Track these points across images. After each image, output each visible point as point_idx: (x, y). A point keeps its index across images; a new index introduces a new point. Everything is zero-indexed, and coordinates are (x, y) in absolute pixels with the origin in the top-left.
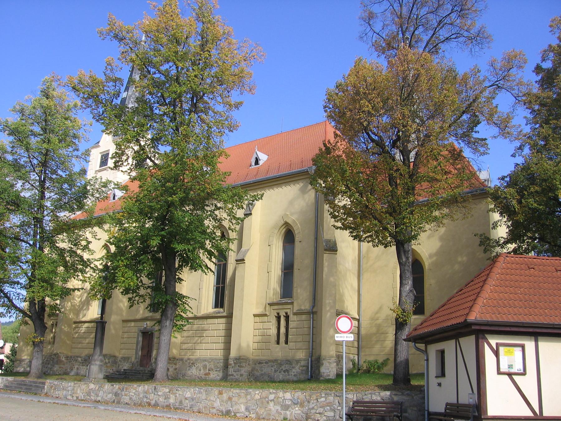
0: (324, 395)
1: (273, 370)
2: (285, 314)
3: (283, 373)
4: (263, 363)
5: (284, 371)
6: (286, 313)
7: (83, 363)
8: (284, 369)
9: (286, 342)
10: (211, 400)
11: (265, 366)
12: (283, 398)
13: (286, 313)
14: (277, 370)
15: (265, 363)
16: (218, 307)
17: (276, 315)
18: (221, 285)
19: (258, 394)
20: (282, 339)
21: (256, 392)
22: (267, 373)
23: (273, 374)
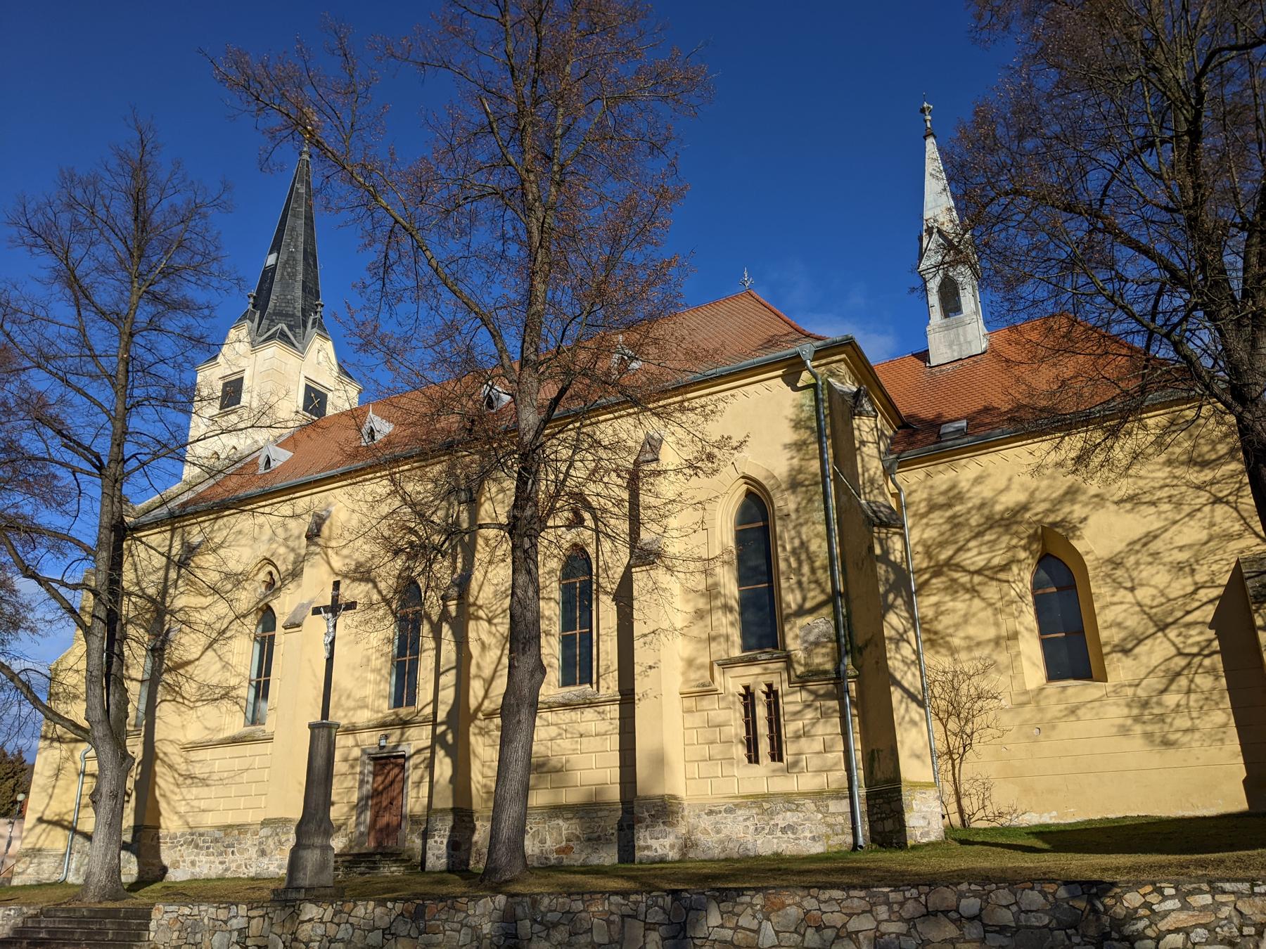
0: (1173, 891)
1: (752, 828)
2: (765, 688)
3: (779, 834)
4: (720, 812)
5: (784, 830)
6: (770, 686)
7: (208, 848)
8: (782, 824)
9: (777, 755)
10: (742, 928)
11: (725, 818)
12: (1014, 908)
13: (770, 686)
14: (763, 829)
15: (726, 811)
16: (574, 684)
17: (743, 691)
18: (262, 679)
19: (916, 899)
20: (764, 746)
21: (908, 894)
22: (734, 837)
23: (749, 838)
